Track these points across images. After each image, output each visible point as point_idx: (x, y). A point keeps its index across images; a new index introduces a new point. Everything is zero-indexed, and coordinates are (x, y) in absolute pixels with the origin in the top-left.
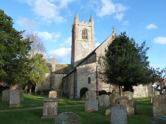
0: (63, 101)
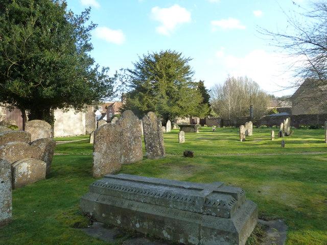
0: (277, 148)
